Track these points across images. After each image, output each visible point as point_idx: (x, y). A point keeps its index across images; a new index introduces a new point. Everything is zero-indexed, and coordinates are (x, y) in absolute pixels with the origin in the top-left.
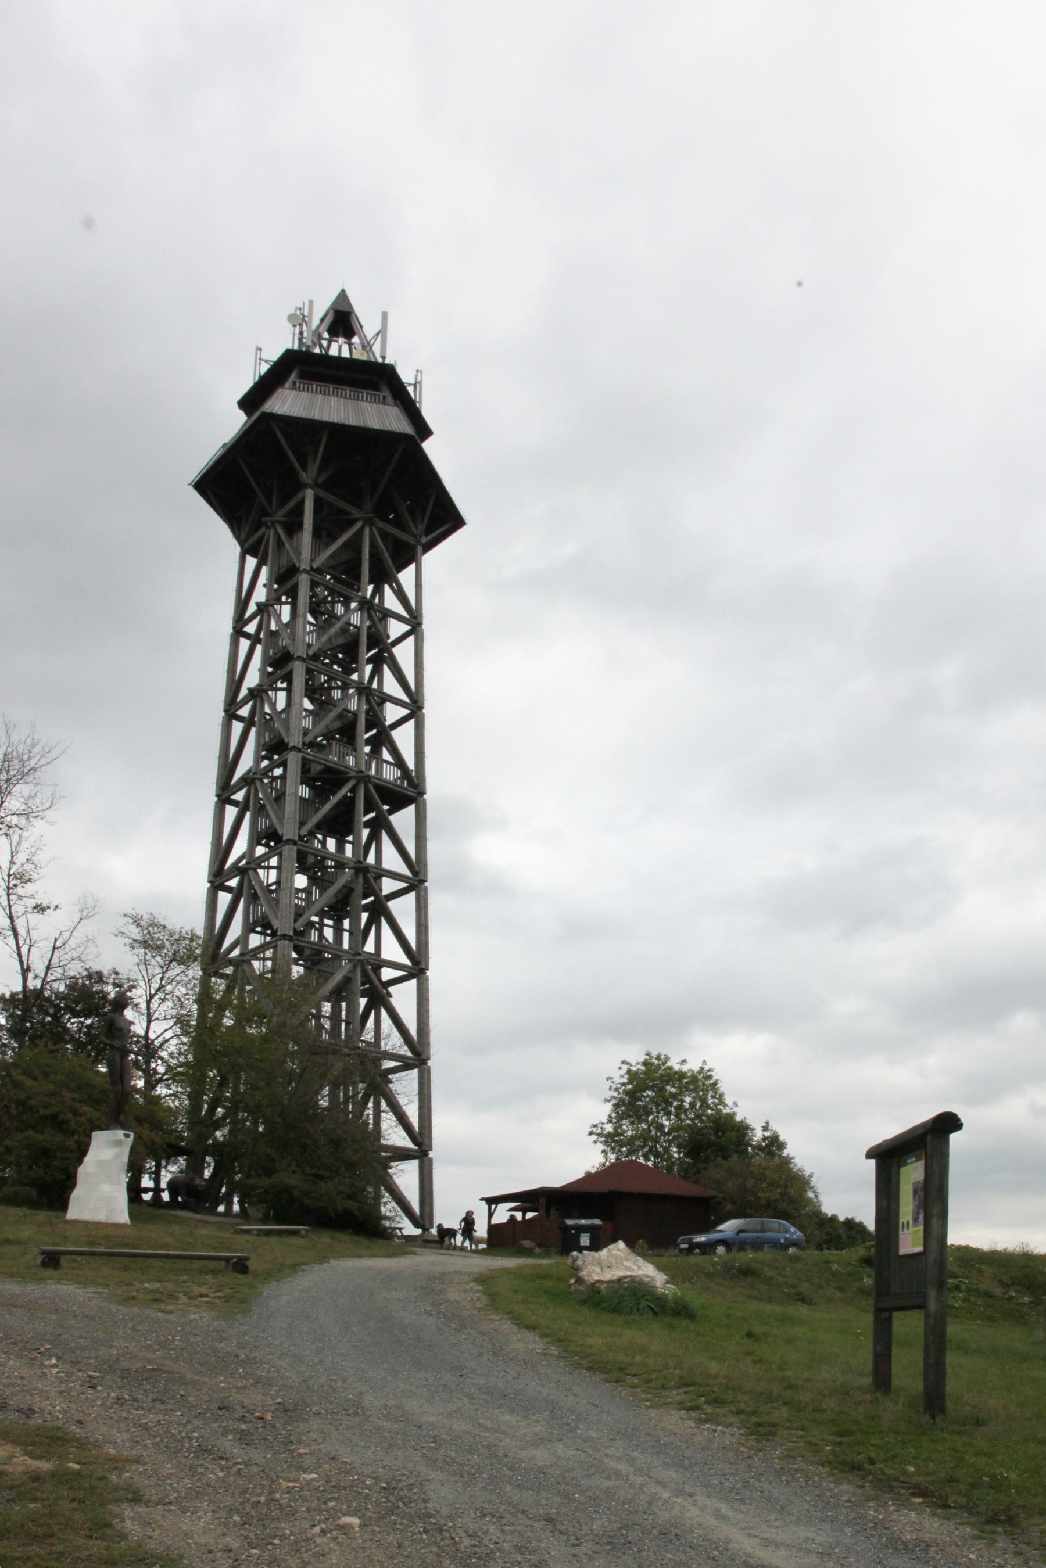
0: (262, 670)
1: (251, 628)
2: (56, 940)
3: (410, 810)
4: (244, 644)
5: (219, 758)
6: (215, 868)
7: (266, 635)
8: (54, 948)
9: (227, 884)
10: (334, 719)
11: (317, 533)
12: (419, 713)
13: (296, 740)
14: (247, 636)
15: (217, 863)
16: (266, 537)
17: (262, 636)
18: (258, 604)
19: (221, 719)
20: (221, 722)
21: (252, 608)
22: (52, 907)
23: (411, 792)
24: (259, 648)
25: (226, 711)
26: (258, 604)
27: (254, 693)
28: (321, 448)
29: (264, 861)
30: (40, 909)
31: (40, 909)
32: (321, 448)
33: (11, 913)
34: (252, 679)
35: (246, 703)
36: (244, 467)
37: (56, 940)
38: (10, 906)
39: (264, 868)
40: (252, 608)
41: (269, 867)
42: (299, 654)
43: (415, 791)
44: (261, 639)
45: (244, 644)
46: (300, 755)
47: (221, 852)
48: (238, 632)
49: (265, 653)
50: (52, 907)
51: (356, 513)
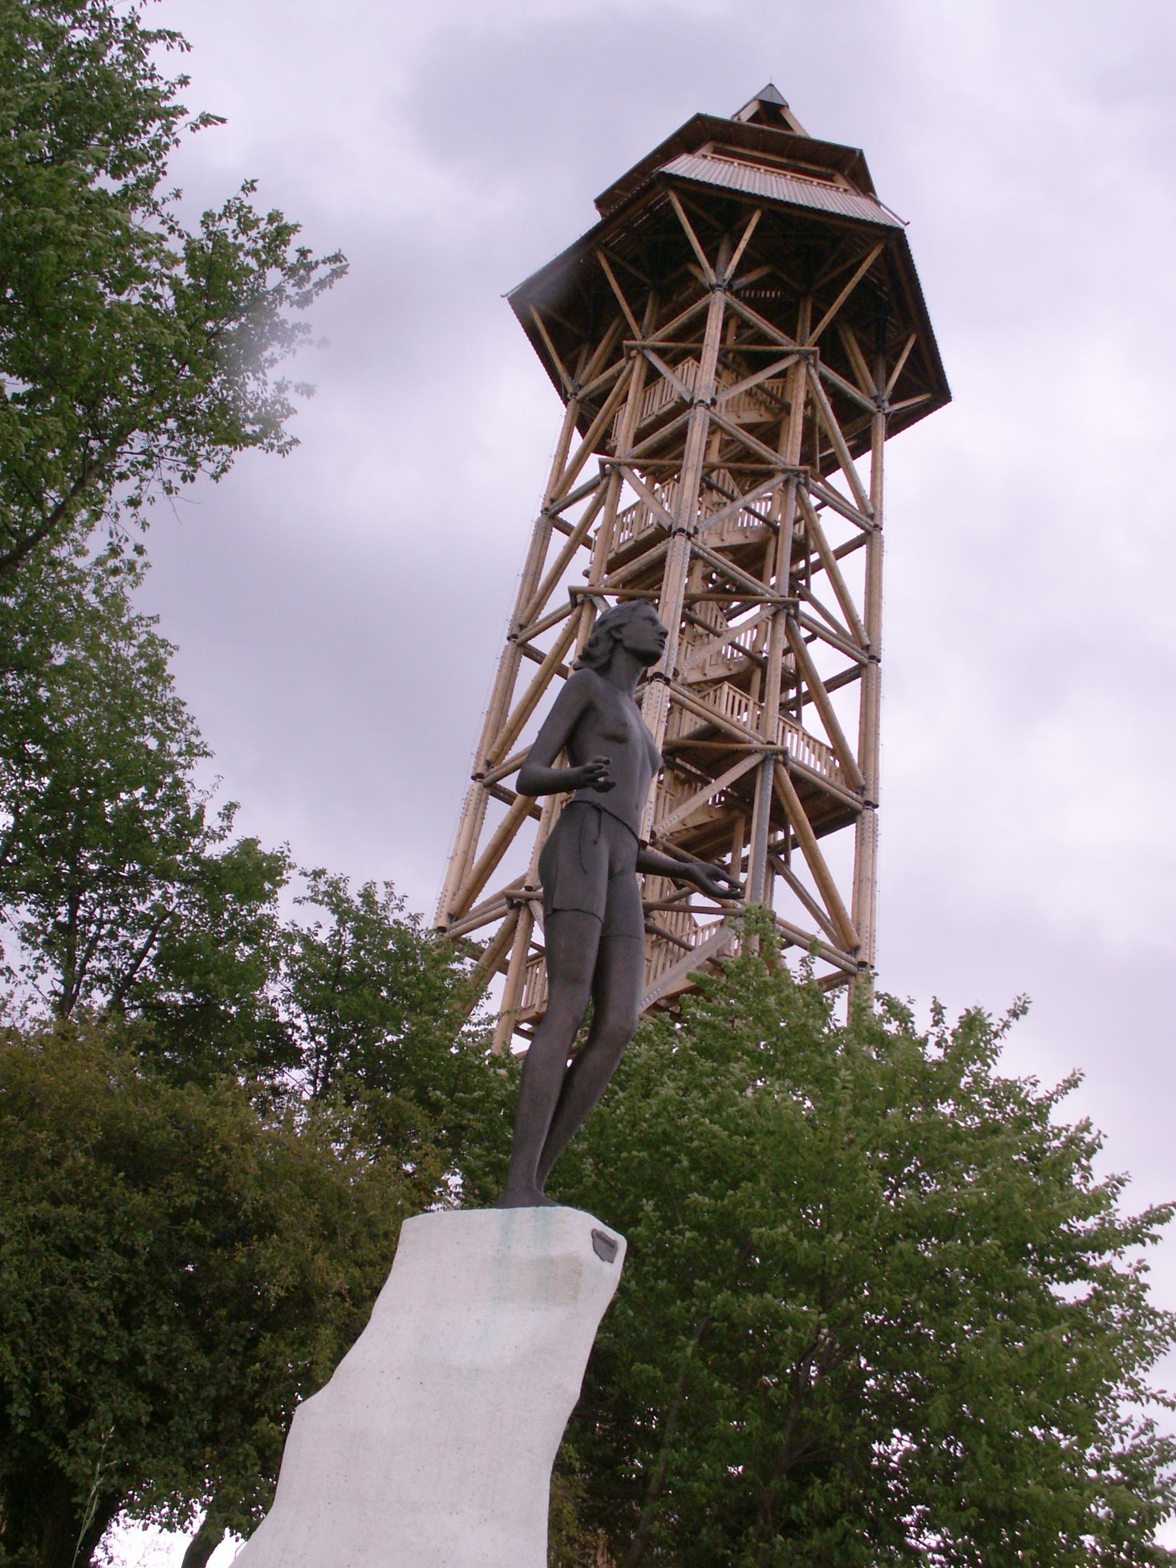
1: (573, 515)
3: (846, 835)
4: (558, 541)
6: (455, 904)
10: (697, 810)
12: (867, 813)
14: (565, 528)
15: (461, 893)
16: (624, 374)
18: (573, 593)
21: (559, 598)
23: (850, 797)
28: (743, 245)
32: (743, 245)
36: (604, 264)
40: (559, 598)
43: (859, 798)
44: (507, 963)
45: (558, 541)
47: (563, 478)
48: (551, 518)
51: (787, 344)
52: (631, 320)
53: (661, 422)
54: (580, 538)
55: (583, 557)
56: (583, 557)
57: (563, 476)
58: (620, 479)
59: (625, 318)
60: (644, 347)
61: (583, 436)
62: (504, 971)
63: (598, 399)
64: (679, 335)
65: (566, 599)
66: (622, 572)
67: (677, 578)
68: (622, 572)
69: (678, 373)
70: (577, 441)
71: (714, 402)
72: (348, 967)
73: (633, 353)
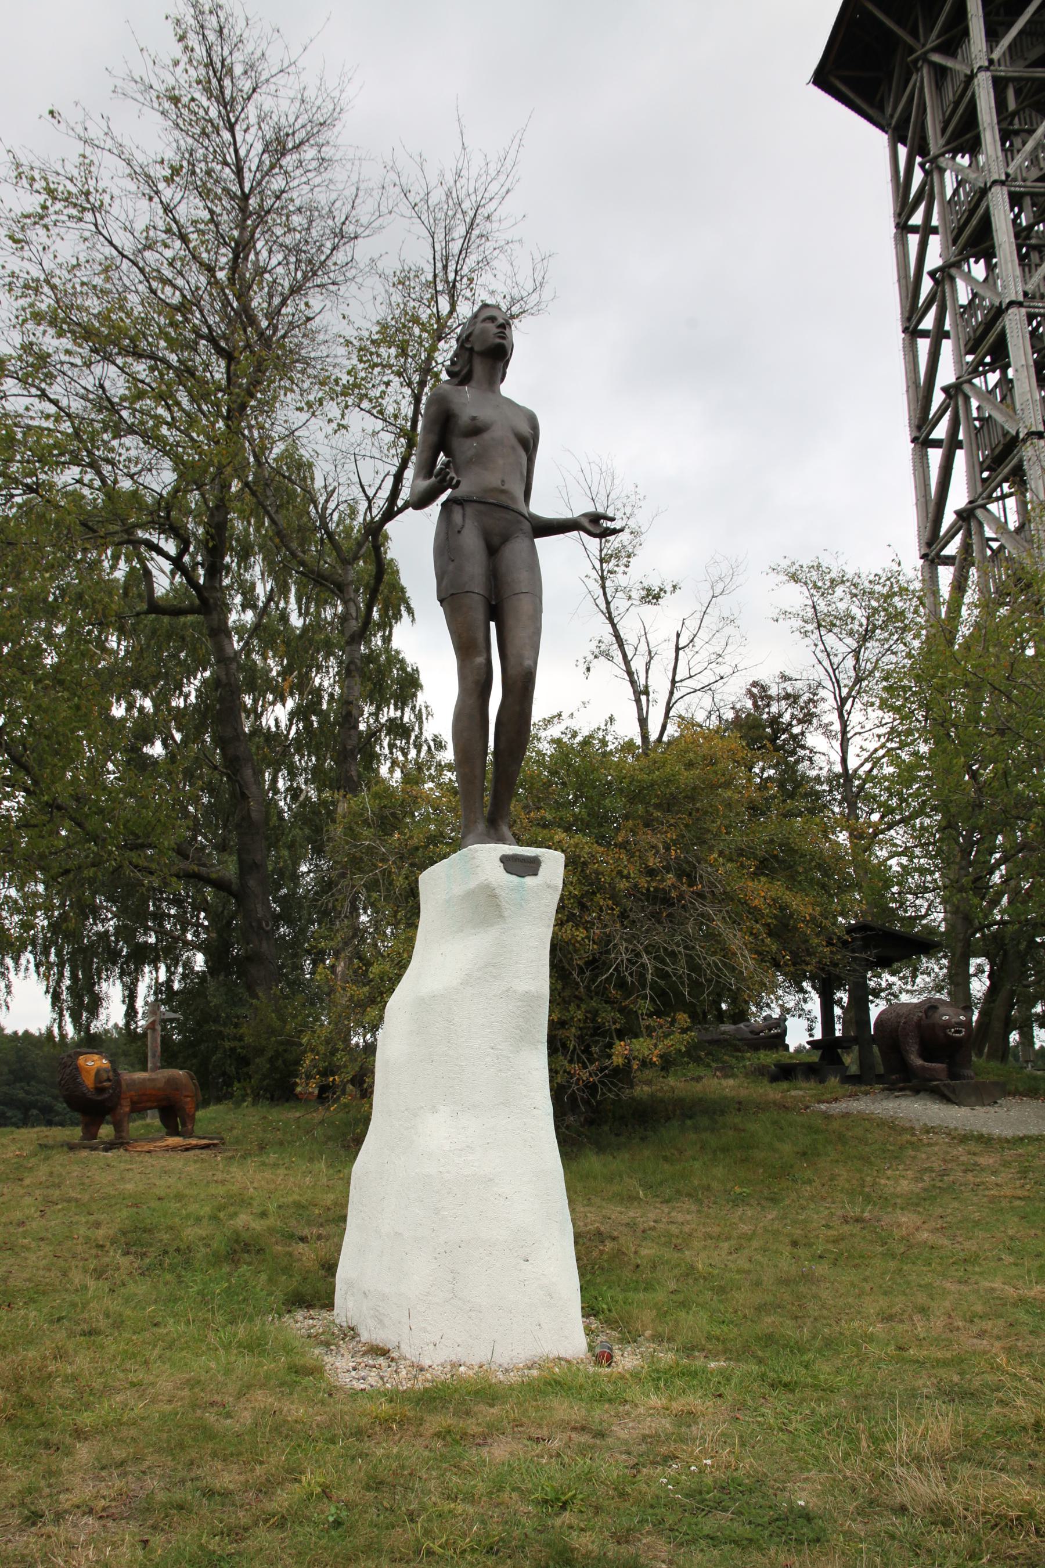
0: (959, 361)
2: (678, 635)
5: (899, 280)
6: (927, 534)
7: (967, 432)
8: (678, 649)
9: (944, 553)
11: (1006, 135)
13: (1013, 291)
17: (961, 437)
18: (945, 390)
19: (901, 342)
20: (901, 346)
21: (938, 398)
22: (669, 588)
24: (960, 456)
25: (905, 330)
26: (945, 390)
27: (965, 516)
29: (995, 490)
30: (652, 596)
31: (652, 596)
33: (610, 613)
34: (958, 497)
35: (953, 537)
37: (678, 635)
38: (608, 603)
39: (998, 499)
41: (1003, 497)
42: (995, 177)
44: (948, 332)
46: (1023, 311)
47: (911, 287)
48: (922, 442)
49: (971, 458)
50: (669, 588)
52: (909, 40)
53: (957, 104)
54: (927, 230)
55: (935, 242)
56: (935, 242)
57: (901, 186)
58: (952, 279)
59: (905, 42)
60: (926, 53)
61: (905, 145)
62: (961, 448)
63: (905, 120)
64: (945, 29)
65: (954, 517)
66: (962, 240)
67: (1002, 216)
68: (962, 240)
69: (959, 57)
70: (903, 151)
71: (991, 62)
72: (924, 749)
73: (920, 64)
